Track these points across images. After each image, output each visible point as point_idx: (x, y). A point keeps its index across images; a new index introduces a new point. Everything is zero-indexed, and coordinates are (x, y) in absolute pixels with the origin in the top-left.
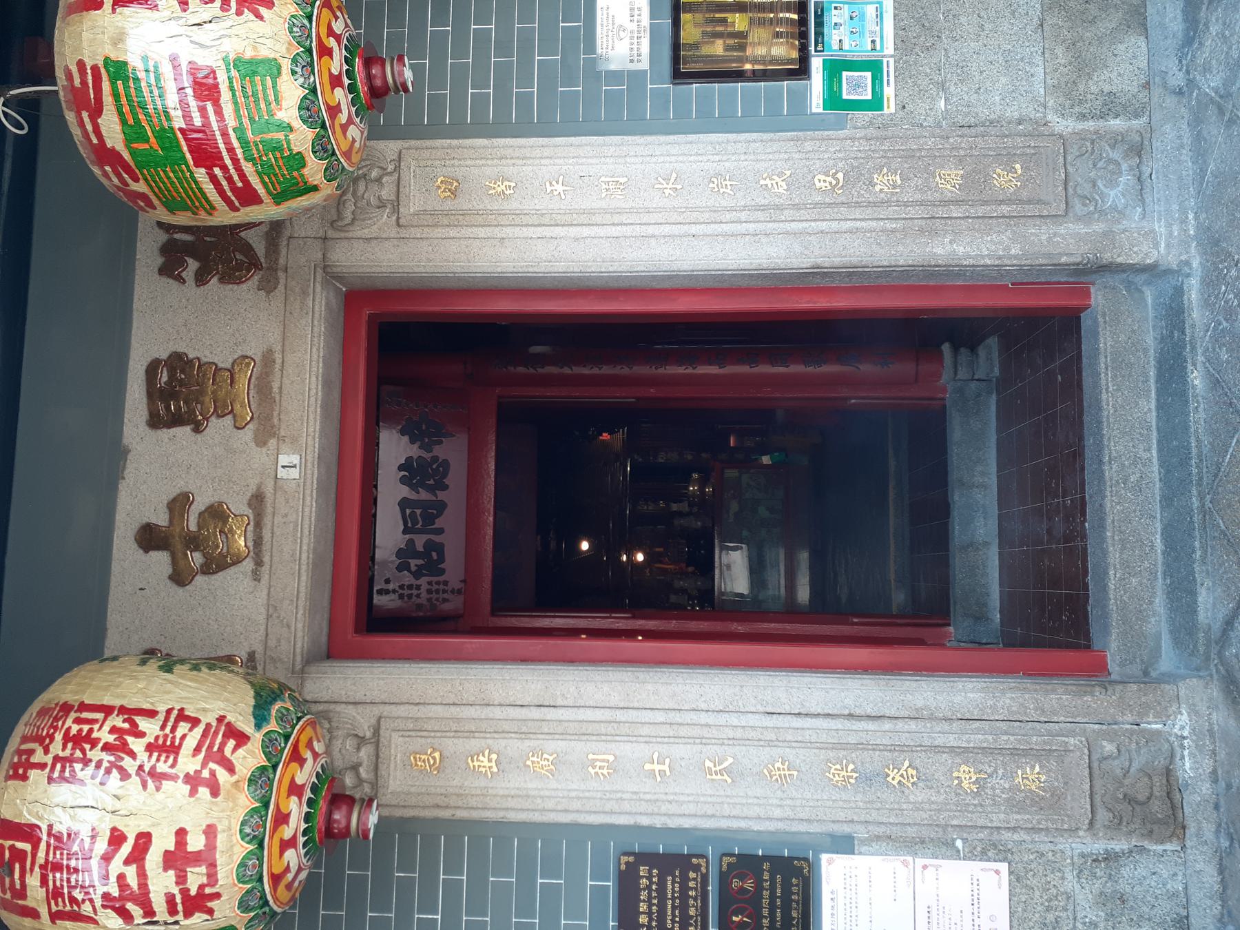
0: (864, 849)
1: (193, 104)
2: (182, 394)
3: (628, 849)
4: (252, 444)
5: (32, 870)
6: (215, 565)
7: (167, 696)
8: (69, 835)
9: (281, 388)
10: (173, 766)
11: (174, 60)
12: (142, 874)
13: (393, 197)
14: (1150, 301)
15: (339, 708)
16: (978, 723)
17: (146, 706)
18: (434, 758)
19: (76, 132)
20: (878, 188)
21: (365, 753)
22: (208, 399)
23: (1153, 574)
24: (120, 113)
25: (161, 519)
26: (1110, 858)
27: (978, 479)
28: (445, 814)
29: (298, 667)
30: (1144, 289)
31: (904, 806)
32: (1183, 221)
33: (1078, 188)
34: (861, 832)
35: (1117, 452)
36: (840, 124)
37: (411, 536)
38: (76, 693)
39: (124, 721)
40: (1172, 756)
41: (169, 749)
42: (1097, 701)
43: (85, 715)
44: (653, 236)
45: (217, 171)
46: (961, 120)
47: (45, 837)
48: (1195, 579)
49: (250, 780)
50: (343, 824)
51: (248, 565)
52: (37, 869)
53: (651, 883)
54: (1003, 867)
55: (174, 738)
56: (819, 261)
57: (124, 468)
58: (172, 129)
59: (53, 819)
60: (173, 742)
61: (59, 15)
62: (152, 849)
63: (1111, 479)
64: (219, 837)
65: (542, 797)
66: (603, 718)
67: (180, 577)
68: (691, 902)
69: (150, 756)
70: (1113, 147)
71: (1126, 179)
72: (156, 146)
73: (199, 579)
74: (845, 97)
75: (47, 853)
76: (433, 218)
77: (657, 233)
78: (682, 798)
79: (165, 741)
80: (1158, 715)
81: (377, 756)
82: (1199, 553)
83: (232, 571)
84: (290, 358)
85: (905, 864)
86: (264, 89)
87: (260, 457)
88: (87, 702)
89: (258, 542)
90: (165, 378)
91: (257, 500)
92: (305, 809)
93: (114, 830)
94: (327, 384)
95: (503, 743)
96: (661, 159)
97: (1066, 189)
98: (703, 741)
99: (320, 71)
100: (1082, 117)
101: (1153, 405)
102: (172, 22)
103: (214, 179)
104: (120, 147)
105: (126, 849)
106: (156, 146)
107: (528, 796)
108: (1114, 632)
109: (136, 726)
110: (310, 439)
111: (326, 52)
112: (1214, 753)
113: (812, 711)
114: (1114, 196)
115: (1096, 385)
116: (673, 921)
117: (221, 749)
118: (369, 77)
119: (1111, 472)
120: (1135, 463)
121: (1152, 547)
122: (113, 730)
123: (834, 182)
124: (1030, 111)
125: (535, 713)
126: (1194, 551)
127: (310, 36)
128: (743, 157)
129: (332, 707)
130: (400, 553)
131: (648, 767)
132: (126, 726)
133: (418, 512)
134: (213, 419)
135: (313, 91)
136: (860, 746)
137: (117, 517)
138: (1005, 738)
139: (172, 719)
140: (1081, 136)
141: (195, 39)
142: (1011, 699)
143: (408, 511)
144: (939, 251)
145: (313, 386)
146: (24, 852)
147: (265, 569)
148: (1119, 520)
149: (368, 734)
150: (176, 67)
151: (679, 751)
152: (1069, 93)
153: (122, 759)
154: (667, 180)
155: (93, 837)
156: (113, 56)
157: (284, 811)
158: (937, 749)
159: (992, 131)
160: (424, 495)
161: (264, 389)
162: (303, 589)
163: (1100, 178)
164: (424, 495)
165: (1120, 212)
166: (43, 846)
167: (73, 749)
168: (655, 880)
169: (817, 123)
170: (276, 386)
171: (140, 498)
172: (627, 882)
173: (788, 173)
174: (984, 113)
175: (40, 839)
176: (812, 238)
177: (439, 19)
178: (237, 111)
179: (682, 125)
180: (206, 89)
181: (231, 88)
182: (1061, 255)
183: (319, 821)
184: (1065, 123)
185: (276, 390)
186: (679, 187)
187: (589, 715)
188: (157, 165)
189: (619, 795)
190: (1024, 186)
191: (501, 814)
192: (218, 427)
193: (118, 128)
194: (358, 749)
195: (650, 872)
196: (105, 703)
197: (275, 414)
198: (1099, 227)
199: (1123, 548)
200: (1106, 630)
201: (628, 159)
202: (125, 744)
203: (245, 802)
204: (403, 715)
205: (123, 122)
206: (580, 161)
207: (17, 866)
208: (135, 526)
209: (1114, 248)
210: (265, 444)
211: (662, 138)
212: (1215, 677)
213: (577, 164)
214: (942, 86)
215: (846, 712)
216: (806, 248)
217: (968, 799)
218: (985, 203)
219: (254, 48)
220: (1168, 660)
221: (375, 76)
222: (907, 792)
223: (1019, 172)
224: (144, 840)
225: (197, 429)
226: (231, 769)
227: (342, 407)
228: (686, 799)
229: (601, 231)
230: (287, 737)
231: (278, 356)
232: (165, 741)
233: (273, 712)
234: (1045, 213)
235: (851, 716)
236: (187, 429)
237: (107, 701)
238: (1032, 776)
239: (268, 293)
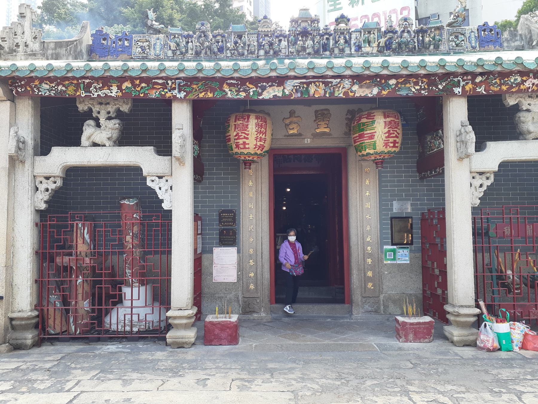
12: (242, 139)
26: (238, 301)
28: (241, 176)
32: (361, 319)
34: (241, 255)
36: (382, 252)
42: (267, 300)
46: (383, 276)
54: (236, 281)
76: (361, 168)
98: (256, 225)
100: (383, 301)
103: (357, 137)
105: (246, 136)
114: (367, 307)
125: (260, 193)
136: (257, 255)
140: (379, 300)
151: (254, 221)
152: (389, 298)
158: (257, 269)
172: (231, 211)
174: (384, 281)
177: (405, 167)
187: (260, 203)
198: (360, 303)
203: (252, 152)
214: (390, 273)
218: (365, 281)
224: (247, 139)
225: (315, 121)
229: (358, 203)
238: (252, 287)
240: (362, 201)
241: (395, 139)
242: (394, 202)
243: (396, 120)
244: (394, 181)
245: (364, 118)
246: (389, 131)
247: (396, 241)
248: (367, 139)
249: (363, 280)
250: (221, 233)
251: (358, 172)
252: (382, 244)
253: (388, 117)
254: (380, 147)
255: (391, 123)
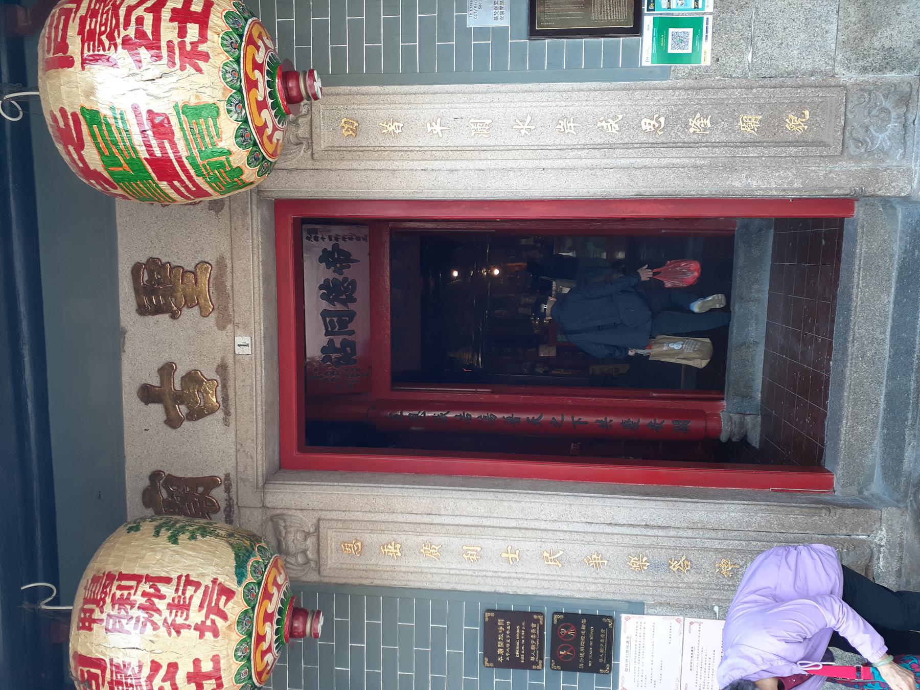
0: (650, 611)
1: (154, 142)
2: (160, 290)
3: (491, 607)
4: (215, 328)
5: (103, 685)
6: (197, 414)
7: (176, 566)
8: (124, 666)
9: (232, 286)
10: (186, 619)
11: (135, 109)
13: (308, 136)
14: (900, 216)
15: (290, 512)
16: (736, 533)
17: (163, 574)
18: (357, 546)
19: (66, 158)
20: (691, 130)
21: (310, 542)
22: (179, 294)
23: (875, 423)
24: (98, 149)
25: (155, 381)
27: (755, 295)
29: (260, 485)
30: (897, 206)
31: (680, 585)
33: (854, 132)
34: (650, 601)
35: (860, 334)
36: (664, 74)
37: (332, 337)
38: (115, 564)
39: (151, 587)
40: (872, 556)
41: (181, 606)
43: (124, 583)
44: (511, 169)
45: (176, 183)
46: (764, 72)
47: (108, 666)
48: (904, 440)
49: (238, 622)
50: (301, 629)
51: (220, 414)
52: (106, 684)
53: (506, 630)
55: (185, 598)
56: (642, 190)
57: (124, 344)
58: (139, 158)
59: (112, 655)
60: (184, 602)
61: (40, 73)
62: (179, 672)
63: (853, 354)
64: (222, 661)
65: (431, 574)
66: (473, 523)
67: (173, 422)
68: (533, 642)
69: (171, 612)
70: (886, 97)
71: (894, 125)
72: (128, 169)
73: (186, 424)
74: (670, 51)
75: (112, 676)
77: (514, 166)
78: (527, 576)
79: (179, 601)
80: (864, 531)
81: (319, 545)
82: (910, 422)
83: (208, 419)
84: (237, 264)
85: (678, 621)
86: (207, 128)
87: (221, 337)
88: (124, 572)
89: (226, 399)
90: (146, 278)
91: (222, 369)
92: (275, 627)
93: (153, 662)
94: (266, 280)
95: (404, 537)
96: (519, 104)
97: (844, 133)
99: (249, 105)
100: (864, 70)
101: (892, 298)
102: (131, 77)
104: (100, 169)
105: (162, 672)
106: (128, 169)
107: (422, 573)
108: (841, 463)
109: (158, 590)
110: (257, 324)
111: (252, 84)
112: (901, 558)
113: (620, 522)
114: (882, 139)
115: (850, 280)
116: (520, 653)
117: (217, 604)
118: (286, 89)
119: (852, 349)
120: (872, 342)
121: (877, 404)
122: (144, 594)
123: (657, 125)
124: (821, 65)
126: (907, 420)
127: (239, 78)
128: (584, 103)
129: (285, 511)
130: (323, 350)
131: (504, 555)
132: (152, 591)
133: (335, 319)
134: (185, 309)
135: (246, 121)
137: (123, 379)
138: (754, 543)
139: (182, 584)
140: (862, 88)
141: (150, 92)
142: (762, 517)
143: (328, 319)
144: (737, 184)
145: (256, 285)
146: (97, 675)
147: (232, 417)
148: (855, 385)
149: (312, 530)
150: (137, 115)
152: (855, 49)
153: (153, 615)
154: (523, 121)
155: (140, 667)
156: (87, 106)
157: (261, 633)
159: (790, 82)
160: (339, 307)
161: (219, 285)
162: (260, 432)
163: (872, 124)
164: (339, 307)
165: (885, 153)
166: (108, 671)
167: (119, 609)
168: (509, 628)
169: (648, 74)
170: (228, 284)
171: (139, 362)
172: (490, 629)
173: (620, 117)
174: (783, 66)
175: (106, 668)
176: (638, 172)
178: (187, 145)
179: (537, 74)
180: (161, 129)
181: (182, 129)
182: (833, 188)
183: (285, 631)
184: (849, 75)
185: (229, 287)
186: (532, 128)
188: (129, 180)
189: (484, 573)
190: (810, 130)
191: (404, 583)
192: (189, 315)
193: (97, 157)
194: (305, 539)
195: (505, 623)
196: (136, 573)
197: (230, 306)
198: (866, 165)
199: (855, 404)
200: (835, 461)
201: (492, 104)
202: (153, 604)
203: (236, 637)
204: (335, 517)
205: (101, 153)
206: (454, 106)
207: (93, 682)
208: (137, 386)
209: (877, 183)
210: (224, 328)
211: (520, 86)
212: (909, 508)
213: (452, 108)
214: (751, 40)
215: (644, 523)
216: (632, 180)
217: (725, 581)
218: (777, 144)
219: (197, 97)
220: (877, 486)
221: (291, 89)
222: (682, 575)
223: (808, 117)
224: (173, 666)
225: (174, 316)
226: (224, 617)
227: (277, 276)
228: (530, 577)
229: (471, 165)
230: (259, 584)
231: (228, 262)
232: (179, 601)
233: (249, 568)
234: (825, 153)
235: (647, 526)
236: (166, 316)
237: (137, 571)
239: (217, 212)
240: (463, 149)
241: (166, 14)
242: (472, 22)
243: (82, 11)
244: (391, 25)
245: (81, 158)
246: (126, 42)
247: (621, 16)
248: (173, 145)
249: (773, 151)
250: (568, 665)
251: (355, 165)
252: (631, 72)
253: (63, 46)
254: (207, 84)
255: (92, 32)
